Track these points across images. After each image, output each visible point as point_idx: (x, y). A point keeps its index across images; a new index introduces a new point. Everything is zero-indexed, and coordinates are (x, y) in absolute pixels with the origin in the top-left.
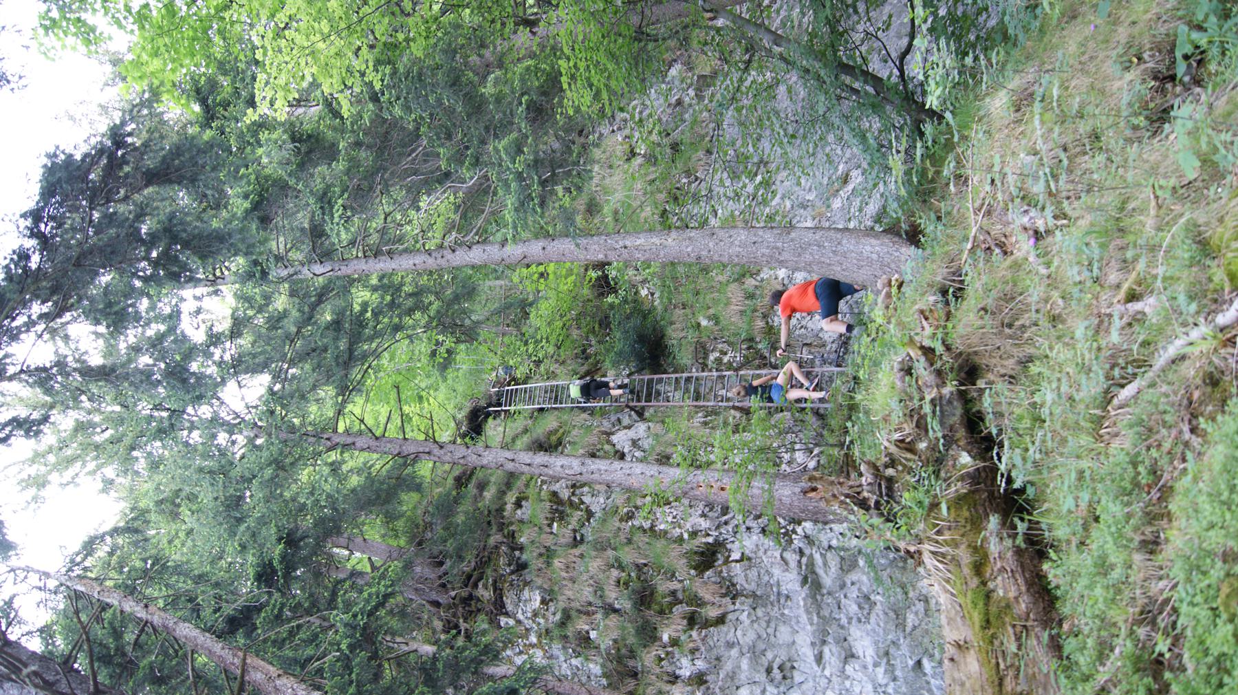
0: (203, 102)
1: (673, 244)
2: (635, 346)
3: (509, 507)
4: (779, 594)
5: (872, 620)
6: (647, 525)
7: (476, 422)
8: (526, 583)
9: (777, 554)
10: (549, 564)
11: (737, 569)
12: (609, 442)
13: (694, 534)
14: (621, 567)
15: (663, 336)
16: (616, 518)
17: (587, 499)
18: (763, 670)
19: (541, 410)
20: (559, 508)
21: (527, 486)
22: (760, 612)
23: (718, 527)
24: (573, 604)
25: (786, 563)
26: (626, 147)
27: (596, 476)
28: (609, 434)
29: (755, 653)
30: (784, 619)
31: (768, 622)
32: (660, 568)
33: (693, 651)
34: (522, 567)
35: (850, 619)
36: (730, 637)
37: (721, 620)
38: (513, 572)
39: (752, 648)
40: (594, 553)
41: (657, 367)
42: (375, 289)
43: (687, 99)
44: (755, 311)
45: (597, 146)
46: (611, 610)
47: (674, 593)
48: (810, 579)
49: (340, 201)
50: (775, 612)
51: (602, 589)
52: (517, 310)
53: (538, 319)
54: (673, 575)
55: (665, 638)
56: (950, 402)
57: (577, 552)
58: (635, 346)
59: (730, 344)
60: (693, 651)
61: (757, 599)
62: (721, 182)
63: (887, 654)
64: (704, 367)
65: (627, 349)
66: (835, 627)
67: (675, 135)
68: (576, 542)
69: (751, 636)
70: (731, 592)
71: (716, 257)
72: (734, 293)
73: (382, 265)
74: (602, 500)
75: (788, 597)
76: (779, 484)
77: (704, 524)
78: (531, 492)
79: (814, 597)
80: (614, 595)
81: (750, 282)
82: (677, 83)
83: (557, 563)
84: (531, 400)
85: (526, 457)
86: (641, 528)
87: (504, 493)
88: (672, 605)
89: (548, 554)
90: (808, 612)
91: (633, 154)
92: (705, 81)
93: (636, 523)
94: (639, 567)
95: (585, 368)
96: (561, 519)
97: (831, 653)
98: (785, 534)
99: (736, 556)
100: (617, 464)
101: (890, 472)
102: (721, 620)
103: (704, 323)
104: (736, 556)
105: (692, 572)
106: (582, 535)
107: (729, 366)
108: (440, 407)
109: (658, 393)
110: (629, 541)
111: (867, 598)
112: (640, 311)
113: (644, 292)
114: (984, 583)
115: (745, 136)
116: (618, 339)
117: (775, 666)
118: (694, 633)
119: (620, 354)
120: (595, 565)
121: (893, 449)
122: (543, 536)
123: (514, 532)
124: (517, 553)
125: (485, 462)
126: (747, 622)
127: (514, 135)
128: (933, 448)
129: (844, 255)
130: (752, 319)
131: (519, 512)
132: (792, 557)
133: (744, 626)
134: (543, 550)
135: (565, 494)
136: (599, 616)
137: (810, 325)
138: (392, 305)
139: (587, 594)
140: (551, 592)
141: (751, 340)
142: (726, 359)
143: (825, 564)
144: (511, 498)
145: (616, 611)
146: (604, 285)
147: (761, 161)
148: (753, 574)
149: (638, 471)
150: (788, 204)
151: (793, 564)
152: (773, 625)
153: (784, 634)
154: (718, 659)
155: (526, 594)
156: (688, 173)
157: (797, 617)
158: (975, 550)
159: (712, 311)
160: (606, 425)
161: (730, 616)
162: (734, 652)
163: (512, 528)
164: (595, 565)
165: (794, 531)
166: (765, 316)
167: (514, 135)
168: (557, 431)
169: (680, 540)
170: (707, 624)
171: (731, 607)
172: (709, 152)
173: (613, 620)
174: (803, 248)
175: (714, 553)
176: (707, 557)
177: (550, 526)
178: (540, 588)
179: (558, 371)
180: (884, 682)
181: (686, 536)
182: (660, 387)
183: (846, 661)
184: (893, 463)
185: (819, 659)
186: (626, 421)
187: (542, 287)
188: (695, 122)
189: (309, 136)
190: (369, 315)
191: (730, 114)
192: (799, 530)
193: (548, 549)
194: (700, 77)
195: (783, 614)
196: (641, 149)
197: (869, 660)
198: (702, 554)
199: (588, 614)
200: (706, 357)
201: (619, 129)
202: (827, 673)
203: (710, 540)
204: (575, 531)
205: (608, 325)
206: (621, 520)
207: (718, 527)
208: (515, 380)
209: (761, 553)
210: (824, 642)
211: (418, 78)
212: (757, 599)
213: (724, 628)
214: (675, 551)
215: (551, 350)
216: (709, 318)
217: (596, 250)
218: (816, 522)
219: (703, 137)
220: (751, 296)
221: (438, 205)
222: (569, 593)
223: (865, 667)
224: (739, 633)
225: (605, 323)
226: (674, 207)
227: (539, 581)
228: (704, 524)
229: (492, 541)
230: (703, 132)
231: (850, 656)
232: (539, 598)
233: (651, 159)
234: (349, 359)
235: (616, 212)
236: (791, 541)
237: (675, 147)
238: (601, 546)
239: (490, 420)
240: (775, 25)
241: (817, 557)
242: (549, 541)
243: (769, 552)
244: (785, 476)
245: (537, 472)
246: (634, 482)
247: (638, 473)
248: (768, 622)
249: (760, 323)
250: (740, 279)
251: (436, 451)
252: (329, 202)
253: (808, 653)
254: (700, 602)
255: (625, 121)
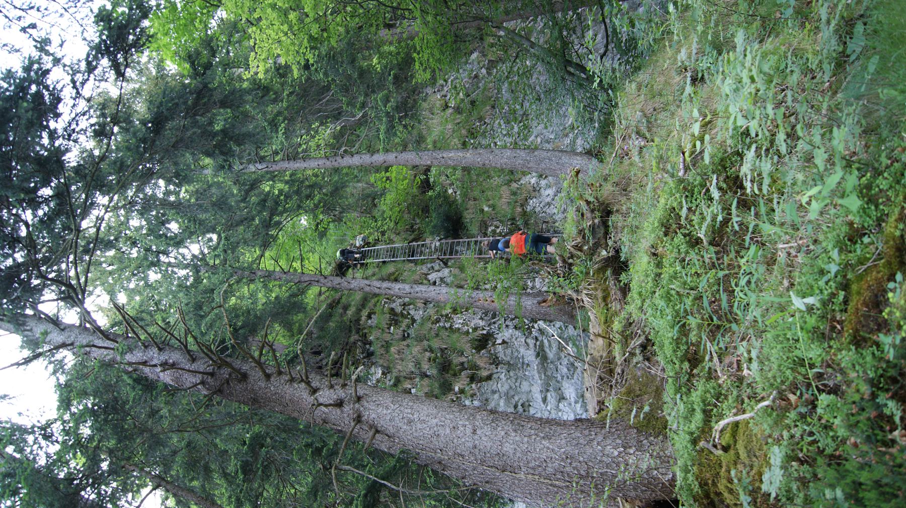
0: (192, 64)
1: (469, 157)
2: (443, 219)
3: (363, 318)
4: (523, 363)
5: (575, 377)
6: (448, 325)
7: (341, 269)
8: (373, 364)
9: (523, 340)
10: (387, 352)
11: (500, 348)
12: (426, 279)
13: (475, 329)
14: (432, 351)
15: (461, 217)
16: (430, 323)
17: (412, 312)
18: (512, 406)
19: (384, 262)
20: (395, 318)
21: (375, 305)
22: (512, 374)
23: (489, 325)
24: (402, 374)
25: (528, 345)
26: (443, 102)
27: (419, 295)
28: (427, 275)
29: (508, 397)
30: (526, 378)
31: (516, 379)
32: (455, 349)
33: (472, 396)
34: (370, 355)
35: (563, 377)
36: (494, 387)
37: (489, 378)
38: (364, 358)
39: (507, 394)
40: (415, 343)
41: (456, 235)
42: (287, 182)
43: (481, 76)
44: (516, 202)
45: (425, 101)
46: (424, 375)
47: (462, 364)
48: (541, 354)
49: (283, 125)
50: (520, 374)
51: (420, 364)
52: (371, 200)
53: (386, 205)
54: (462, 354)
55: (457, 389)
56: (598, 227)
57: (405, 343)
58: (443, 219)
59: (501, 221)
60: (472, 396)
61: (510, 366)
62: (499, 124)
63: (583, 396)
64: (485, 235)
65: (439, 224)
66: (554, 381)
67: (473, 96)
68: (404, 338)
69: (506, 387)
70: (495, 361)
71: (493, 165)
72: (505, 191)
73: (298, 165)
74: (421, 313)
75: (528, 365)
76: (524, 299)
77: (482, 323)
78: (378, 309)
79: (543, 364)
80: (427, 367)
81: (514, 185)
82: (476, 63)
83: (393, 350)
84: (377, 257)
85: (378, 284)
86: (444, 327)
87: (361, 310)
88: (461, 371)
89: (387, 346)
90: (539, 373)
91: (447, 107)
92: (492, 64)
93: (442, 324)
94: (442, 350)
95: (412, 237)
96: (396, 324)
97: (551, 397)
98: (528, 329)
99: (499, 341)
100: (432, 288)
101: (571, 261)
102: (489, 378)
103: (486, 209)
104: (499, 341)
105: (474, 351)
106: (408, 334)
107: (500, 234)
108: (318, 259)
109: (457, 252)
110: (437, 335)
111: (573, 364)
112: (448, 201)
113: (450, 191)
114: (607, 305)
115: (516, 99)
116: (434, 218)
117: (519, 404)
118: (473, 386)
119: (434, 227)
120: (416, 349)
121: (572, 249)
122: (385, 335)
123: (366, 334)
124: (368, 346)
125: (352, 286)
126: (504, 379)
127: (386, 92)
128: (589, 248)
129: (563, 165)
130: (514, 207)
131: (369, 321)
132: (531, 342)
133: (502, 382)
134: (384, 343)
135: (399, 309)
136: (417, 380)
137: (548, 211)
138: (298, 192)
139: (411, 367)
140: (388, 368)
141: (514, 219)
142: (498, 231)
143: (550, 346)
144: (365, 313)
145: (427, 376)
146: (426, 185)
147: (524, 114)
148: (509, 351)
149: (444, 291)
150: (539, 140)
151: (532, 346)
152: (519, 381)
153: (525, 386)
154: (487, 400)
155: (373, 369)
156: (481, 119)
157: (533, 376)
158: (604, 291)
159: (491, 202)
160: (425, 270)
161: (494, 376)
162: (496, 396)
163: (366, 331)
164: (416, 350)
165: (533, 327)
166: (522, 205)
167: (386, 92)
168: (394, 273)
169: (468, 333)
170: (481, 380)
171: (496, 371)
172: (493, 107)
173: (426, 381)
174: (541, 160)
175: (487, 341)
176: (483, 342)
177: (389, 328)
178: (381, 366)
179: (395, 239)
180: (580, 412)
181: (471, 330)
182: (459, 248)
183: (559, 401)
184: (572, 257)
185: (545, 400)
186: (437, 268)
187: (387, 186)
188: (484, 89)
189: (265, 87)
190: (282, 198)
191: (505, 86)
192: (536, 326)
193: (387, 342)
194: (490, 61)
195: (525, 375)
196: (452, 104)
197: (573, 400)
198: (480, 340)
199: (411, 379)
200: (487, 229)
201: (439, 91)
202: (549, 408)
203: (485, 332)
204: (404, 331)
205: (428, 211)
206: (433, 323)
207: (489, 325)
208: (368, 244)
209: (513, 340)
210: (548, 391)
211: (332, 57)
212: (510, 366)
213: (491, 383)
214: (465, 339)
215: (392, 225)
216: (489, 206)
217: (425, 159)
218: (545, 320)
219: (490, 98)
220: (514, 194)
221: (326, 133)
222: (399, 367)
223: (570, 404)
224: (499, 385)
225: (426, 210)
226: (471, 136)
227: (381, 362)
228: (482, 323)
229: (352, 339)
230: (490, 95)
231: (562, 398)
232: (380, 372)
233: (458, 110)
234: (267, 225)
235: (435, 142)
236: (531, 333)
237: (473, 103)
238: (420, 339)
239: (350, 270)
240: (533, 39)
241: (546, 341)
242: (388, 337)
243: (519, 339)
244: (529, 294)
245: (384, 292)
246: (442, 298)
247: (443, 293)
248: (516, 379)
249: (519, 209)
250: (509, 183)
251: (322, 280)
252: (275, 125)
253: (538, 397)
254: (476, 367)
255: (442, 86)
